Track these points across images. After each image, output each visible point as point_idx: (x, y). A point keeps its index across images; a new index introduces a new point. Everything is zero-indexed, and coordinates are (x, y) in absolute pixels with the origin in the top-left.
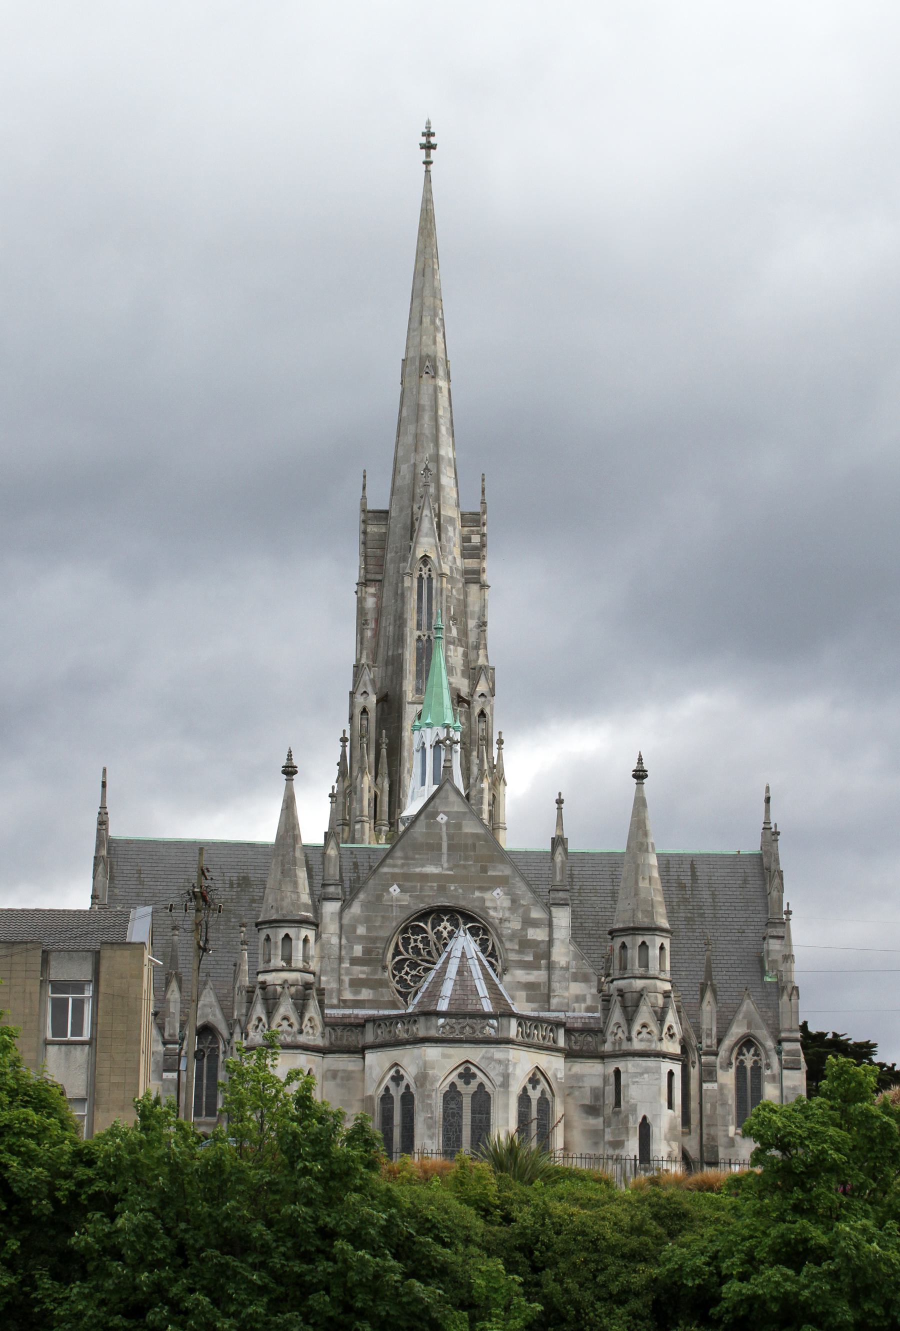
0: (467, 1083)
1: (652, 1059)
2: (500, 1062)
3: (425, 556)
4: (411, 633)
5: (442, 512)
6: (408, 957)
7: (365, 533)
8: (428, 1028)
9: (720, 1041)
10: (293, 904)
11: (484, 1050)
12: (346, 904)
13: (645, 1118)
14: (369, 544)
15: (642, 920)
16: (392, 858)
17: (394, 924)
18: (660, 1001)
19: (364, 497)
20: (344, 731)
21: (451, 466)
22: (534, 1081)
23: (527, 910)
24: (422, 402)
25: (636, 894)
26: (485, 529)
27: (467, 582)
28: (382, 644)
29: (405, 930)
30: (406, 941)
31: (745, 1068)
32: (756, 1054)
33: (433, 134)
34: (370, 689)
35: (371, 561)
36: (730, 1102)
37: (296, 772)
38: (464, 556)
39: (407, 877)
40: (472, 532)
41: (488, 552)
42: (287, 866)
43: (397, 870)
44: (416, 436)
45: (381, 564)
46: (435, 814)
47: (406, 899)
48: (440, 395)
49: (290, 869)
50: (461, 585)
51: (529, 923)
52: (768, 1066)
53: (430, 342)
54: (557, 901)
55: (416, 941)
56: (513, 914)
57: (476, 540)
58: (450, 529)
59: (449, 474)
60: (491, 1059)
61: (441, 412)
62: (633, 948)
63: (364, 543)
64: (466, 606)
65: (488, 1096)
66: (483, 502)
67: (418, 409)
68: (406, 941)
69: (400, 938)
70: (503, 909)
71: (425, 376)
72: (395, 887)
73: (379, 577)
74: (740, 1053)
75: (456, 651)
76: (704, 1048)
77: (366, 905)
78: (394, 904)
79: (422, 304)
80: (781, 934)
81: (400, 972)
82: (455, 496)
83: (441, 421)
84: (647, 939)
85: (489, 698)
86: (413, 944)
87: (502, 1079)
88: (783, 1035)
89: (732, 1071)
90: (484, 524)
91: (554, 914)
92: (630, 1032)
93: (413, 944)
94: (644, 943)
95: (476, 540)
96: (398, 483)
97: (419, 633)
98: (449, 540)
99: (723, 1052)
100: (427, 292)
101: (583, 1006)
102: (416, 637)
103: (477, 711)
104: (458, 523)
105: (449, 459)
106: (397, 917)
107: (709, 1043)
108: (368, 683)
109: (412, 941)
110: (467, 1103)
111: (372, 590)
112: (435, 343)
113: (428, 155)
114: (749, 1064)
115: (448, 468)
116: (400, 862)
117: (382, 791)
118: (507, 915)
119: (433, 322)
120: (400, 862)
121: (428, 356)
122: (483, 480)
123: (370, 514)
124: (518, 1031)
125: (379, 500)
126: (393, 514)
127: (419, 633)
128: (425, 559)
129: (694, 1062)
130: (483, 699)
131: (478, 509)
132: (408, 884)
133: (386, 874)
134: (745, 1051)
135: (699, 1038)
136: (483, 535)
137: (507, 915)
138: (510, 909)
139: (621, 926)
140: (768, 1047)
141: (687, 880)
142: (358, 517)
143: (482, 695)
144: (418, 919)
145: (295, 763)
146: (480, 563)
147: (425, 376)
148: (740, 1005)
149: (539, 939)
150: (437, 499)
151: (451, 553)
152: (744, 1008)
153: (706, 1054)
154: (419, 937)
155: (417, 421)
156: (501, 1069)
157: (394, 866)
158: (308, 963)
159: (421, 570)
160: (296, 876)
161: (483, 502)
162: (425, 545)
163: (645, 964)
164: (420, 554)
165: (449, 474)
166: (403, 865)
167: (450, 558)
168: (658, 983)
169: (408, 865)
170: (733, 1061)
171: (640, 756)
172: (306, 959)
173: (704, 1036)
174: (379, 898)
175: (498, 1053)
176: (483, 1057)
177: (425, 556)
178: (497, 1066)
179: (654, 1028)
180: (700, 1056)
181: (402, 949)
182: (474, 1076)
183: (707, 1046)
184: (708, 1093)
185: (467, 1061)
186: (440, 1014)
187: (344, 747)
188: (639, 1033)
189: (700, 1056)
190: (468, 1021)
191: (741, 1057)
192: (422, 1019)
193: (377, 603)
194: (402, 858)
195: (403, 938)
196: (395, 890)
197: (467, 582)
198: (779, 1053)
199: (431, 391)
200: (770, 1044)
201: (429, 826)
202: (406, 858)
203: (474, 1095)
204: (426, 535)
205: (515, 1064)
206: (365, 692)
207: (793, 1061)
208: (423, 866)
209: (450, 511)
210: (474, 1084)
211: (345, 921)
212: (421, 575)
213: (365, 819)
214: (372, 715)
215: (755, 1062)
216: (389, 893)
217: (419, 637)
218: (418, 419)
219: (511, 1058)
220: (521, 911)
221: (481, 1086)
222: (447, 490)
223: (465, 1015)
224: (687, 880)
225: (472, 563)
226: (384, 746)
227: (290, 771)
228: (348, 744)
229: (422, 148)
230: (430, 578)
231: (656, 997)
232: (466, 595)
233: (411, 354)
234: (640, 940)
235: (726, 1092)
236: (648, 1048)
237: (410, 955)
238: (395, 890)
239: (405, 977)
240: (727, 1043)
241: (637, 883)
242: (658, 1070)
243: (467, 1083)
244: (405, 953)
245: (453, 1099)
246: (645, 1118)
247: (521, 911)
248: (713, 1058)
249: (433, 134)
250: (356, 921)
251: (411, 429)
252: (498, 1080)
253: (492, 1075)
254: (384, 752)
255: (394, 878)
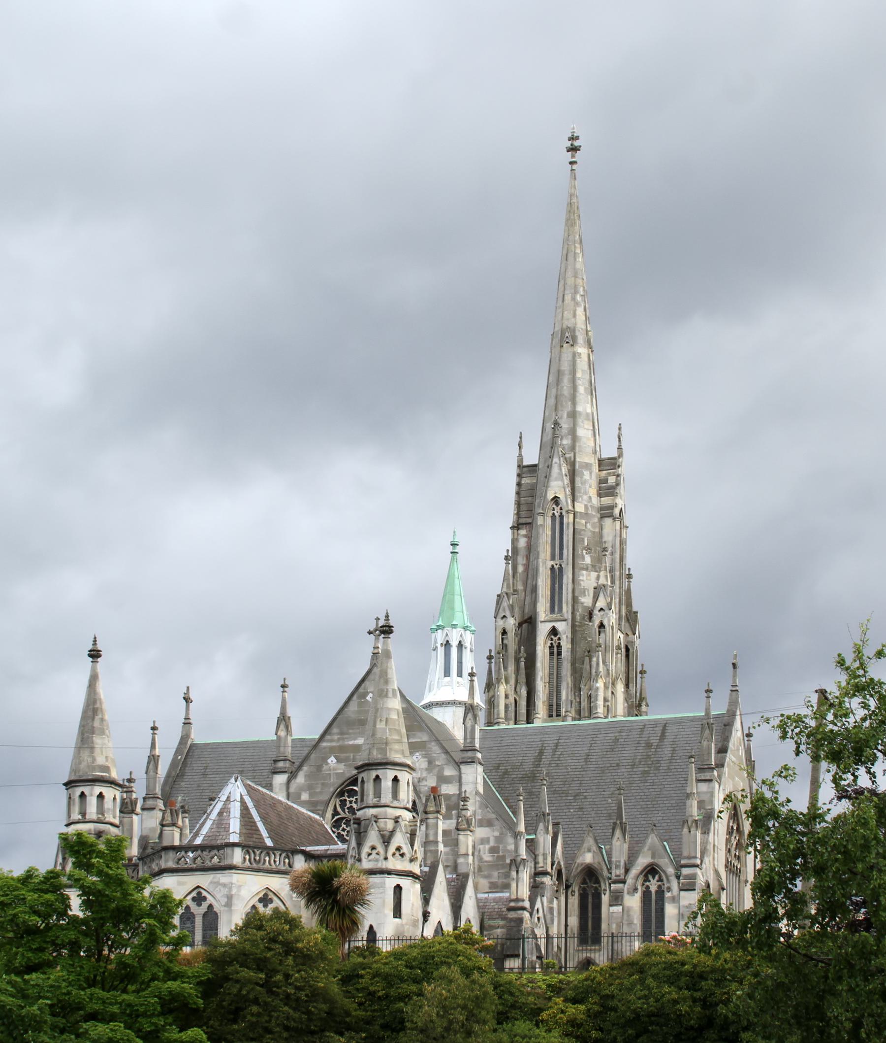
0: (199, 905)
1: (378, 875)
2: (224, 885)
3: (556, 497)
4: (545, 563)
5: (578, 459)
6: (344, 816)
7: (519, 484)
8: (166, 861)
9: (627, 871)
10: (88, 766)
11: (212, 876)
12: (293, 775)
13: (371, 927)
14: (523, 493)
15: (376, 756)
16: (330, 734)
17: (332, 789)
18: (390, 825)
19: (520, 455)
20: (490, 651)
21: (589, 420)
22: (265, 901)
23: (441, 769)
24: (562, 368)
25: (373, 735)
26: (620, 471)
27: (602, 517)
28: (530, 576)
29: (341, 794)
30: (343, 803)
31: (651, 892)
32: (660, 880)
33: (577, 138)
34: (508, 614)
35: (523, 508)
36: (635, 921)
37: (100, 656)
38: (600, 495)
39: (342, 749)
40: (609, 474)
41: (621, 490)
42: (86, 735)
43: (334, 744)
44: (556, 397)
45: (531, 510)
46: (365, 694)
47: (341, 768)
48: (578, 360)
49: (88, 738)
50: (596, 520)
51: (443, 779)
52: (669, 889)
53: (571, 316)
54: (465, 760)
55: (351, 802)
56: (429, 773)
57: (612, 480)
58: (586, 474)
59: (586, 426)
60: (218, 884)
61: (579, 375)
62: (368, 781)
63: (518, 493)
64: (601, 536)
65: (216, 914)
66: (620, 448)
67: (559, 373)
68: (343, 803)
69: (338, 800)
70: (421, 769)
71: (565, 345)
72: (332, 758)
73: (529, 520)
74: (646, 880)
75: (589, 575)
76: (614, 877)
77: (308, 776)
78: (332, 772)
79: (565, 284)
80: (708, 778)
81: (338, 829)
82: (593, 445)
83: (579, 382)
84: (380, 772)
85: (607, 611)
86: (348, 805)
87: (226, 900)
88: (683, 862)
89: (638, 896)
90: (619, 466)
91: (463, 771)
92: (359, 854)
93: (348, 805)
94: (377, 777)
95: (612, 480)
96: (544, 440)
97: (552, 563)
98: (584, 483)
99: (630, 880)
100: (569, 273)
101: (487, 847)
102: (549, 566)
103: (597, 623)
104: (596, 468)
105: (587, 414)
106: (334, 783)
107: (618, 873)
108: (507, 608)
109: (348, 803)
110: (199, 921)
111: (523, 532)
112: (575, 316)
113: (573, 156)
114: (653, 889)
115: (586, 422)
116: (336, 737)
117: (520, 696)
118: (425, 774)
119: (574, 299)
120: (336, 737)
121: (568, 328)
122: (620, 429)
123: (525, 469)
124: (245, 859)
125: (531, 457)
126: (541, 466)
127: (552, 563)
128: (556, 500)
129: (605, 890)
130: (602, 613)
131: (616, 455)
132: (343, 755)
133: (325, 748)
134: (650, 877)
135: (609, 870)
136: (618, 476)
137: (425, 774)
138: (427, 769)
139: (361, 763)
140: (669, 873)
141: (655, 741)
142: (514, 471)
143: (602, 609)
144: (349, 785)
145: (99, 647)
146: (614, 500)
147: (565, 345)
148: (647, 837)
149: (451, 793)
150: (573, 448)
151: (586, 493)
152: (650, 840)
153: (615, 882)
154: (354, 799)
155: (558, 385)
156: (225, 891)
157: (332, 741)
158: (103, 815)
159: (554, 509)
160: (93, 743)
161: (620, 448)
162: (557, 487)
163: (378, 794)
164: (550, 496)
165: (586, 426)
166: (339, 739)
167: (585, 497)
168: (389, 810)
169: (343, 739)
170: (639, 887)
171: (387, 613)
172: (101, 810)
173: (613, 867)
174: (319, 768)
175: (223, 877)
176: (211, 882)
177: (556, 497)
178: (222, 889)
179: (380, 849)
180: (610, 884)
181: (339, 809)
182: (205, 899)
183: (617, 876)
184: (614, 915)
185: (198, 887)
186: (195, 848)
187: (490, 663)
188: (370, 855)
189: (610, 884)
190: (215, 852)
191: (648, 883)
192: (163, 854)
193: (527, 542)
194: (338, 734)
195: (341, 801)
196: (332, 760)
197: (602, 517)
198: (678, 877)
199: (570, 358)
200: (671, 870)
201: (360, 705)
202: (342, 733)
203: (205, 915)
204: (556, 480)
205: (240, 886)
206: (504, 616)
207: (689, 884)
208: (355, 739)
209: (585, 457)
210: (205, 905)
211: (292, 790)
212: (554, 514)
213: (501, 720)
214: (511, 635)
215: (659, 887)
216: (328, 764)
217: (553, 566)
218: (558, 382)
219: (234, 881)
220: (436, 771)
221: (210, 906)
222: (584, 440)
223: (220, 847)
224: (655, 741)
225: (606, 501)
226: (522, 659)
227: (95, 654)
228: (493, 661)
229: (568, 151)
230: (561, 516)
231: (386, 822)
232: (601, 528)
233: (556, 329)
234: (373, 774)
235: (632, 913)
236: (375, 867)
237: (346, 814)
238: (332, 760)
239: (342, 833)
240: (635, 871)
241: (375, 725)
242: (383, 885)
243: (199, 905)
244: (342, 813)
245: (188, 919)
246: (371, 927)
247: (436, 771)
248: (621, 885)
249: (577, 138)
250: (301, 789)
251: (553, 392)
252: (224, 901)
253: (218, 896)
254: (522, 664)
255: (332, 751)
